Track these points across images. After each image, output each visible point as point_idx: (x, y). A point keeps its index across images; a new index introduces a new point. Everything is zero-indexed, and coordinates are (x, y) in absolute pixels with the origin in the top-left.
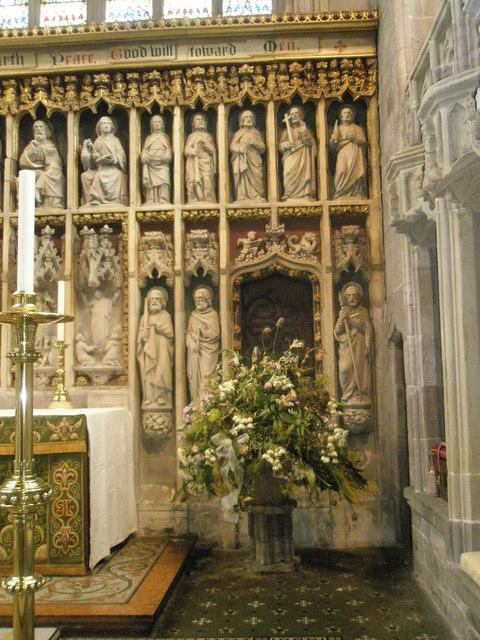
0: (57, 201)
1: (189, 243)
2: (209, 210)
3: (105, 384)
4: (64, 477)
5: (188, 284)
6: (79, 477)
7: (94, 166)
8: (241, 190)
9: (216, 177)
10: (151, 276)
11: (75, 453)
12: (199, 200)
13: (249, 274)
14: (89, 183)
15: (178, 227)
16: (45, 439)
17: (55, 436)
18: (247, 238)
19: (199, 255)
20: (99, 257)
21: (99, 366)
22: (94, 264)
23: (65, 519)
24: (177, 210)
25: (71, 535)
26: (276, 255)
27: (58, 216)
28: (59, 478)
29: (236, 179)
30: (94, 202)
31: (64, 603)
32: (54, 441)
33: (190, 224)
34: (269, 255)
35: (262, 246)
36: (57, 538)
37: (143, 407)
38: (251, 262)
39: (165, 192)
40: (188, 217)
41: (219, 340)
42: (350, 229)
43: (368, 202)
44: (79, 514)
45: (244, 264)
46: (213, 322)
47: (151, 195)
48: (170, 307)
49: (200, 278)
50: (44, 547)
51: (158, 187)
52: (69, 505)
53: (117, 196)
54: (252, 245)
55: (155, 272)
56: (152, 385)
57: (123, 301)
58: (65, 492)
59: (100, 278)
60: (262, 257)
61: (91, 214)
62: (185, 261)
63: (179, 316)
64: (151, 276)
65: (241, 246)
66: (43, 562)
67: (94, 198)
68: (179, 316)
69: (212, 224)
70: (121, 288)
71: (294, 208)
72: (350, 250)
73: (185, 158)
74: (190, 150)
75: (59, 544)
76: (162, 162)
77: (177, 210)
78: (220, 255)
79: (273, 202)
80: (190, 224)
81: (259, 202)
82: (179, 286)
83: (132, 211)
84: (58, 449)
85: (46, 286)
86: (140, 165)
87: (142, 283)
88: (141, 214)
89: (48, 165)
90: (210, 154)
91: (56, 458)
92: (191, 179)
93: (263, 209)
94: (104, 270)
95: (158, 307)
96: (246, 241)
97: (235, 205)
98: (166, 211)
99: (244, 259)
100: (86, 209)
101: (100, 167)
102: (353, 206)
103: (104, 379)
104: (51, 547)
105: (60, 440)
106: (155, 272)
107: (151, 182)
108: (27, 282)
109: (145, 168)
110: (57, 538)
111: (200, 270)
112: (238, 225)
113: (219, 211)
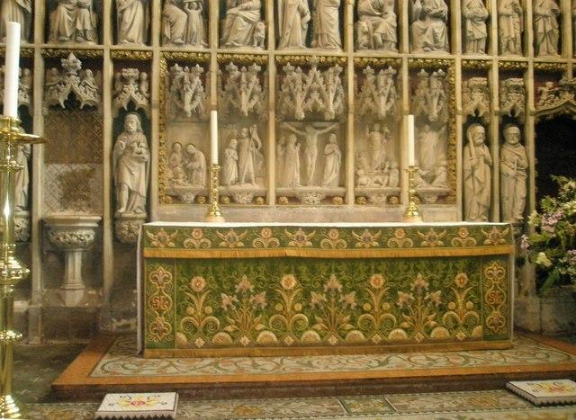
0: (393, 45)
1: (503, 89)
2: (520, 62)
3: (436, 203)
4: (495, 273)
5: (116, 115)
6: (173, 279)
7: (423, 15)
8: (543, 46)
9: (523, 35)
10: (474, 115)
11: (504, 254)
12: (512, 53)
13: (545, 116)
14: (421, 31)
15: (495, 74)
16: (481, 243)
17: (487, 241)
18: (545, 86)
19: (514, 100)
20: (249, 92)
21: (431, 188)
22: (299, 99)
23: (160, 312)
24: (494, 60)
25: (165, 325)
26: (568, 103)
27: (395, 59)
28: (491, 274)
29: (540, 38)
30: (426, 49)
31: (150, 377)
32: (222, 247)
33: (505, 73)
34: (563, 101)
35: (557, 94)
36: (153, 327)
37: (117, 215)
38: (550, 107)
39: (483, 45)
40: (502, 66)
41: (528, 170)
42: (478, 81)
43: (401, 55)
44: (173, 308)
45: (544, 108)
46: (520, 156)
47: (471, 46)
48: (488, 142)
49: (509, 119)
50: (479, 328)
51: (478, 40)
52: (499, 294)
53: (443, 45)
54: (550, 93)
55: (477, 112)
56: (479, 204)
57: (448, 135)
58: (495, 284)
59: (306, 112)
60: (558, 103)
61: (424, 59)
62: (501, 103)
63: (496, 147)
64: (474, 115)
65: (541, 93)
66: (478, 339)
67: (426, 45)
68: (496, 147)
69: (520, 72)
70: (448, 124)
71: (305, 56)
72: (478, 97)
73: (499, 16)
74: (503, 10)
75: (492, 325)
76: (482, 19)
77: (494, 60)
78: (535, 102)
79: (530, 58)
80: (505, 73)
81: (557, 58)
82: (495, 122)
83: (458, 57)
84: (491, 251)
85: (25, 111)
86: (464, 19)
87: (465, 120)
88: (465, 62)
89: (386, 13)
90: (519, 16)
91: (487, 259)
92: (506, 35)
93: (561, 64)
94: (253, 103)
95: (481, 141)
96: (546, 90)
97: (50, 45)
98: (485, 61)
99: (543, 104)
100: (419, 54)
101: (428, 19)
102: (480, 61)
103: (434, 199)
104: (485, 327)
105: (492, 244)
106: (477, 112)
107: (473, 36)
108: (12, 112)
109: (469, 23)
110: (153, 327)
111: (513, 112)
112: (542, 75)
113: (527, 63)
